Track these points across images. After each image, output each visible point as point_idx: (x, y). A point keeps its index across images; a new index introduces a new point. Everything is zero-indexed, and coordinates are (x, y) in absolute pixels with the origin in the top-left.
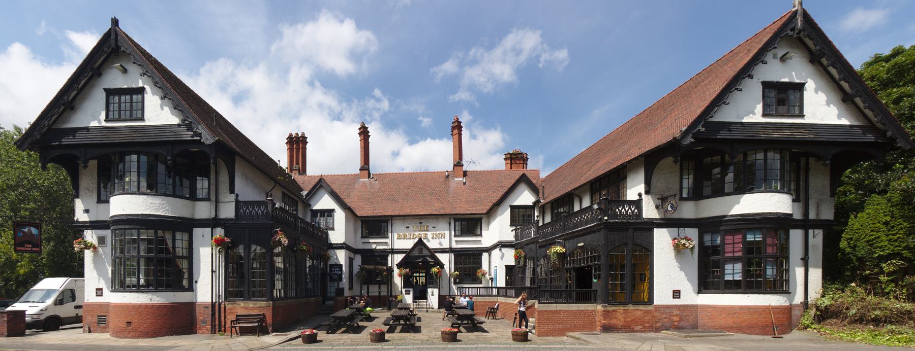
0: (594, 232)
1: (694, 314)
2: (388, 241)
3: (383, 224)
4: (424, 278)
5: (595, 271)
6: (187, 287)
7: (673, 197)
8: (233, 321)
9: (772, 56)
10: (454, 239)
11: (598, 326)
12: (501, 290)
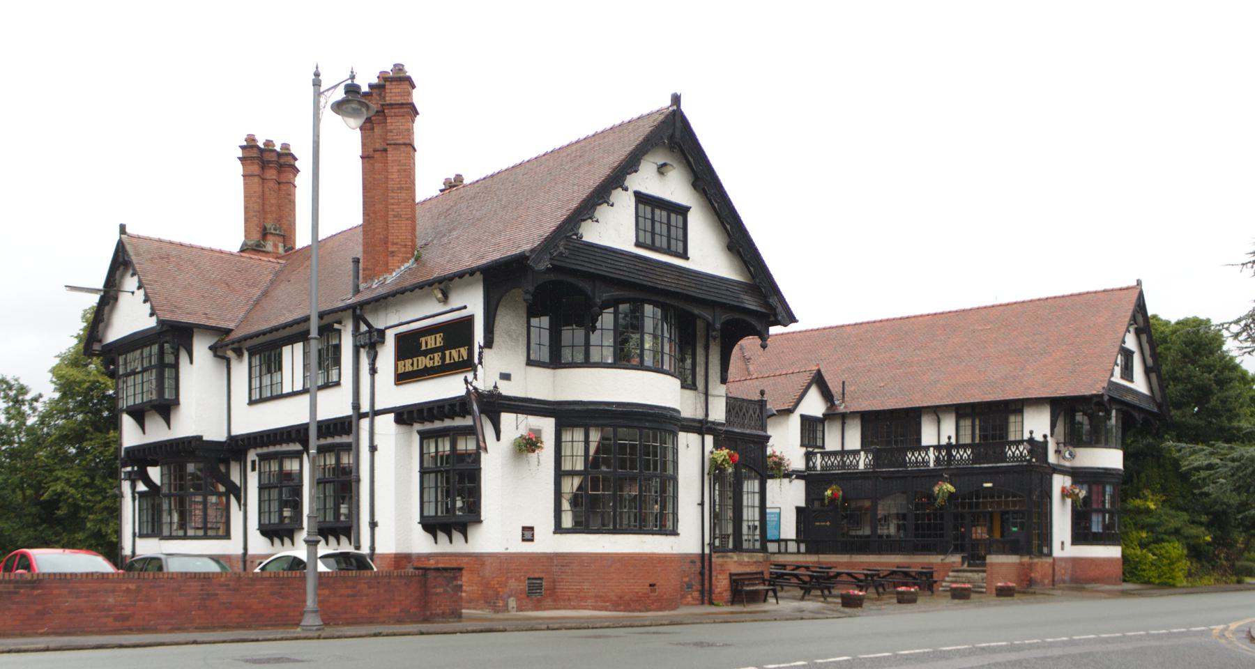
9: (661, 162)
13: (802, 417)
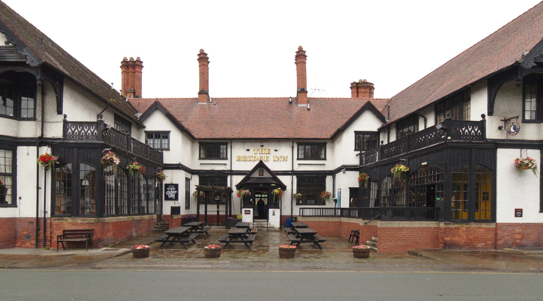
0: (438, 151)
1: (536, 233)
2: (227, 162)
3: (222, 147)
4: (266, 199)
5: (438, 190)
6: (10, 203)
7: (516, 118)
8: (60, 236)
10: (296, 162)
11: (441, 243)
12: (345, 211)
13: (357, 133)
